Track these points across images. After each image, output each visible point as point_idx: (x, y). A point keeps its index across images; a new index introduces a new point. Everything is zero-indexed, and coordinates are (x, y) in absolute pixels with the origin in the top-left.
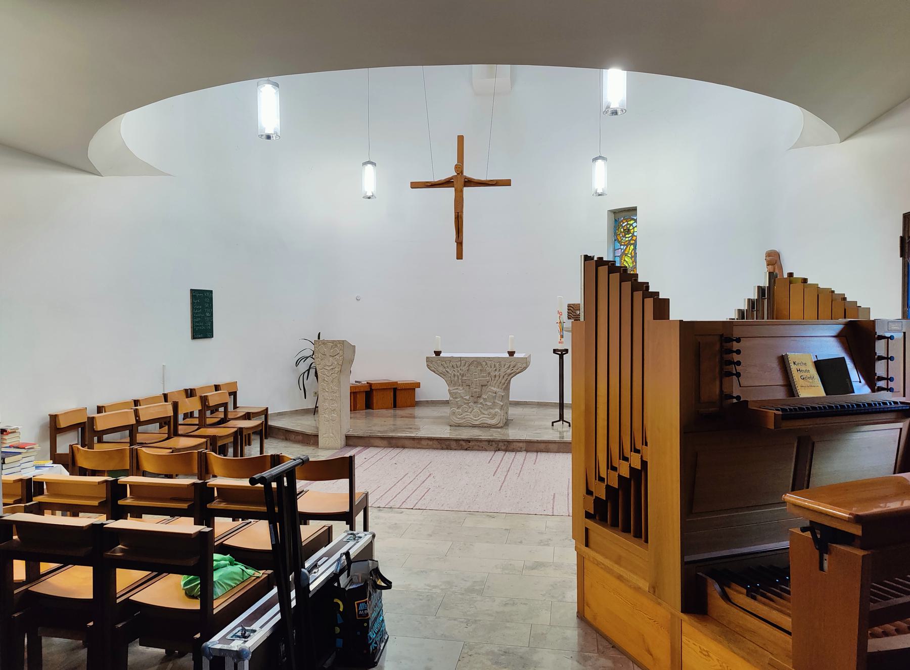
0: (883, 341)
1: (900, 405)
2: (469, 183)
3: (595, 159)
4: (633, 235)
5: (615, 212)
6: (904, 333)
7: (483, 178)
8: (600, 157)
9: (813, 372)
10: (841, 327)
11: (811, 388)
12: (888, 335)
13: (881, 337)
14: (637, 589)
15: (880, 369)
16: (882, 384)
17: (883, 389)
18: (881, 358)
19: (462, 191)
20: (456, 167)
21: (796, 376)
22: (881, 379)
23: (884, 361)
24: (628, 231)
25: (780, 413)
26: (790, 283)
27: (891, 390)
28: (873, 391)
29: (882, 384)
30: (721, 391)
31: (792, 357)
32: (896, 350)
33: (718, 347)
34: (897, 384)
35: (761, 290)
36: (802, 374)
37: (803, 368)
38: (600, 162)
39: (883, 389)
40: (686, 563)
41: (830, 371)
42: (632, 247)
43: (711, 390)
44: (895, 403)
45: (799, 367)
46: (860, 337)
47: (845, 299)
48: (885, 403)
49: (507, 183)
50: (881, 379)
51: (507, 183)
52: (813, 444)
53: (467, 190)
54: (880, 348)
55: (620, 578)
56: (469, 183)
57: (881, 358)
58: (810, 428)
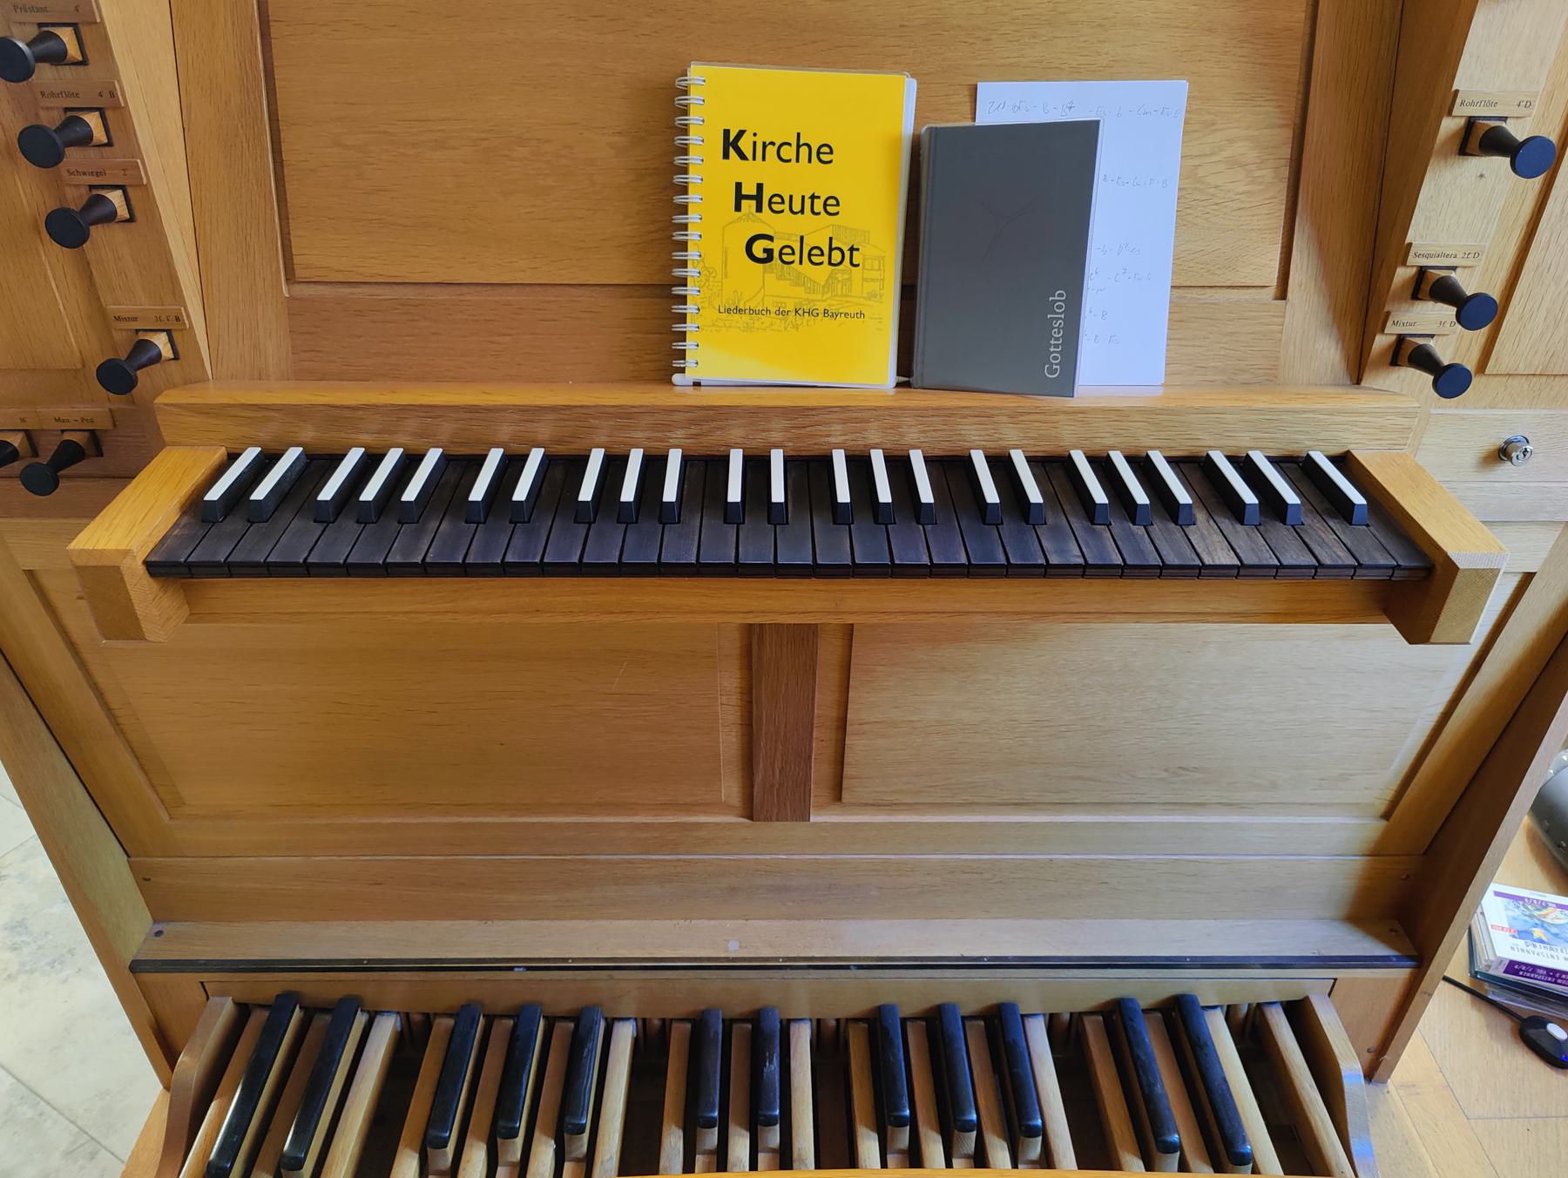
11: (794, 336)
15: (1460, 215)
29: (1431, 322)
36: (766, 222)
39: (1423, 359)
45: (749, 174)
57: (1484, 139)
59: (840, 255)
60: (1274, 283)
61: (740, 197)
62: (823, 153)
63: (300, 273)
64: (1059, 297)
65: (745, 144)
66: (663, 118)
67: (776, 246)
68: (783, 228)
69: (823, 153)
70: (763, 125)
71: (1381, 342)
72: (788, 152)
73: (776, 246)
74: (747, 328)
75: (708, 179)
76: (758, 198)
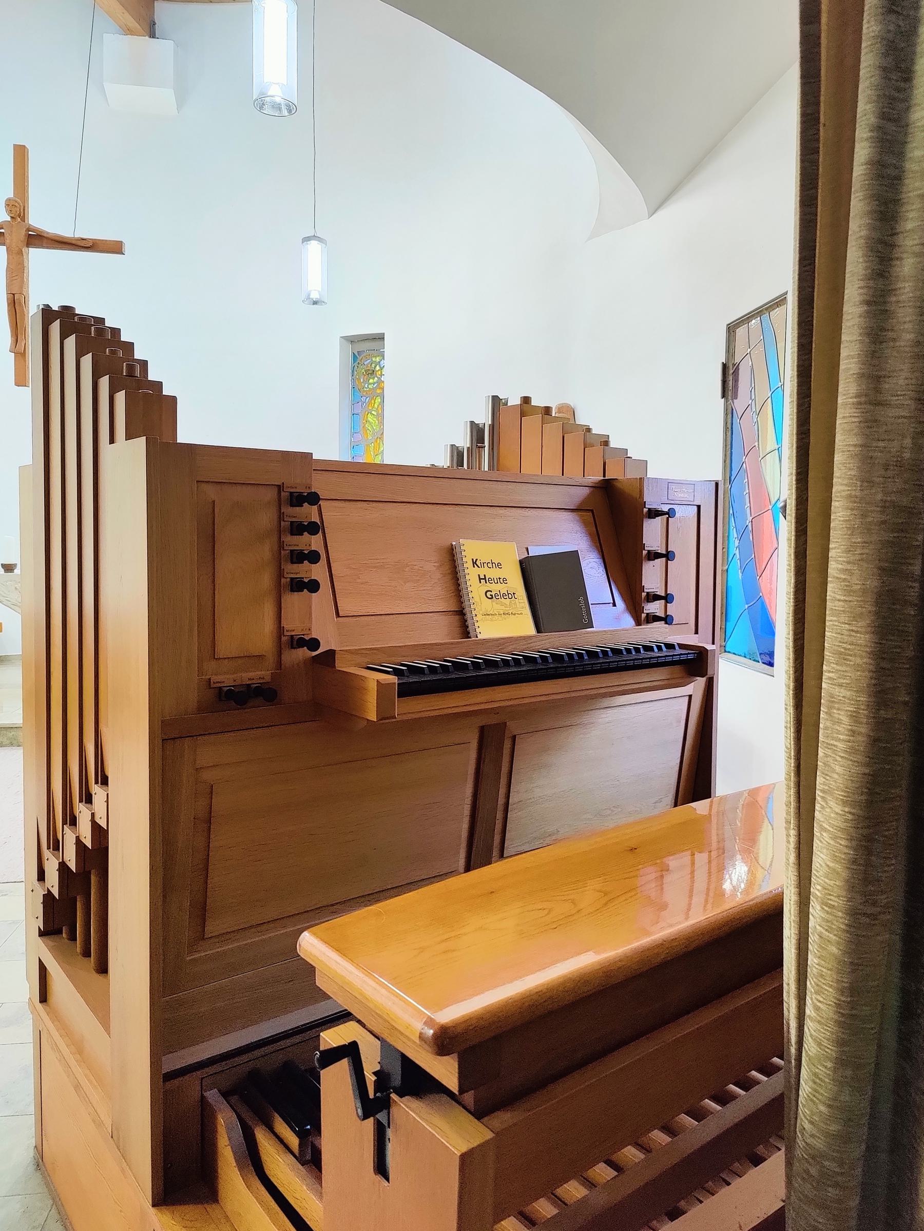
0: (659, 521)
1: (678, 651)
2: (37, 239)
3: (307, 239)
4: (380, 382)
5: (352, 340)
6: (699, 507)
7: (66, 232)
8: (314, 237)
9: (516, 583)
10: (586, 491)
11: (504, 622)
12: (665, 508)
13: (654, 514)
14: (99, 1124)
15: (651, 577)
16: (655, 608)
17: (656, 619)
18: (654, 556)
19: (20, 253)
20: (10, 205)
21: (475, 591)
22: (654, 597)
23: (660, 562)
24: (372, 373)
25: (393, 679)
26: (523, 414)
27: (667, 620)
28: (638, 623)
29: (655, 608)
30: (280, 630)
31: (470, 549)
32: (682, 543)
33: (266, 519)
34: (682, 609)
35: (477, 432)
36: (489, 586)
37: (492, 573)
38: (314, 243)
39: (656, 619)
40: (169, 1077)
41: (549, 585)
42: (378, 400)
43: (248, 631)
44: (670, 646)
45: (482, 572)
46: (617, 513)
47: (606, 443)
48: (648, 648)
49: (116, 248)
50: (654, 597)
51: (116, 248)
52: (514, 738)
53: (36, 256)
54: (652, 534)
55: (78, 1087)
56: (37, 239)
57: (654, 556)
58: (489, 709)
59: (511, 595)
60: (32, 1109)
61: (480, 579)
62: (499, 565)
63: (341, 614)
64: (581, 599)
65: (478, 563)
66: (452, 558)
67: (493, 594)
68: (495, 588)
69: (499, 565)
70: (483, 558)
71: (644, 616)
72: (490, 565)
73: (493, 594)
74: (492, 620)
75: (471, 575)
76: (485, 579)
